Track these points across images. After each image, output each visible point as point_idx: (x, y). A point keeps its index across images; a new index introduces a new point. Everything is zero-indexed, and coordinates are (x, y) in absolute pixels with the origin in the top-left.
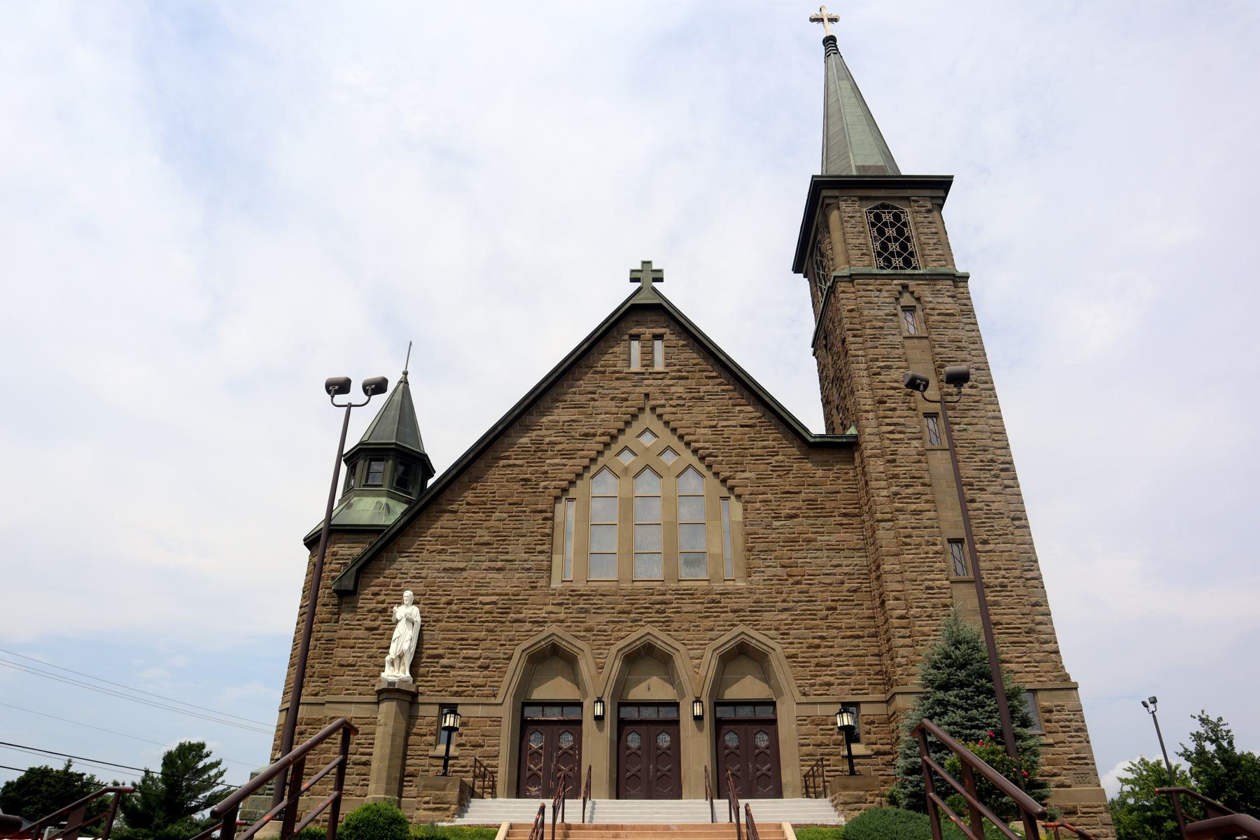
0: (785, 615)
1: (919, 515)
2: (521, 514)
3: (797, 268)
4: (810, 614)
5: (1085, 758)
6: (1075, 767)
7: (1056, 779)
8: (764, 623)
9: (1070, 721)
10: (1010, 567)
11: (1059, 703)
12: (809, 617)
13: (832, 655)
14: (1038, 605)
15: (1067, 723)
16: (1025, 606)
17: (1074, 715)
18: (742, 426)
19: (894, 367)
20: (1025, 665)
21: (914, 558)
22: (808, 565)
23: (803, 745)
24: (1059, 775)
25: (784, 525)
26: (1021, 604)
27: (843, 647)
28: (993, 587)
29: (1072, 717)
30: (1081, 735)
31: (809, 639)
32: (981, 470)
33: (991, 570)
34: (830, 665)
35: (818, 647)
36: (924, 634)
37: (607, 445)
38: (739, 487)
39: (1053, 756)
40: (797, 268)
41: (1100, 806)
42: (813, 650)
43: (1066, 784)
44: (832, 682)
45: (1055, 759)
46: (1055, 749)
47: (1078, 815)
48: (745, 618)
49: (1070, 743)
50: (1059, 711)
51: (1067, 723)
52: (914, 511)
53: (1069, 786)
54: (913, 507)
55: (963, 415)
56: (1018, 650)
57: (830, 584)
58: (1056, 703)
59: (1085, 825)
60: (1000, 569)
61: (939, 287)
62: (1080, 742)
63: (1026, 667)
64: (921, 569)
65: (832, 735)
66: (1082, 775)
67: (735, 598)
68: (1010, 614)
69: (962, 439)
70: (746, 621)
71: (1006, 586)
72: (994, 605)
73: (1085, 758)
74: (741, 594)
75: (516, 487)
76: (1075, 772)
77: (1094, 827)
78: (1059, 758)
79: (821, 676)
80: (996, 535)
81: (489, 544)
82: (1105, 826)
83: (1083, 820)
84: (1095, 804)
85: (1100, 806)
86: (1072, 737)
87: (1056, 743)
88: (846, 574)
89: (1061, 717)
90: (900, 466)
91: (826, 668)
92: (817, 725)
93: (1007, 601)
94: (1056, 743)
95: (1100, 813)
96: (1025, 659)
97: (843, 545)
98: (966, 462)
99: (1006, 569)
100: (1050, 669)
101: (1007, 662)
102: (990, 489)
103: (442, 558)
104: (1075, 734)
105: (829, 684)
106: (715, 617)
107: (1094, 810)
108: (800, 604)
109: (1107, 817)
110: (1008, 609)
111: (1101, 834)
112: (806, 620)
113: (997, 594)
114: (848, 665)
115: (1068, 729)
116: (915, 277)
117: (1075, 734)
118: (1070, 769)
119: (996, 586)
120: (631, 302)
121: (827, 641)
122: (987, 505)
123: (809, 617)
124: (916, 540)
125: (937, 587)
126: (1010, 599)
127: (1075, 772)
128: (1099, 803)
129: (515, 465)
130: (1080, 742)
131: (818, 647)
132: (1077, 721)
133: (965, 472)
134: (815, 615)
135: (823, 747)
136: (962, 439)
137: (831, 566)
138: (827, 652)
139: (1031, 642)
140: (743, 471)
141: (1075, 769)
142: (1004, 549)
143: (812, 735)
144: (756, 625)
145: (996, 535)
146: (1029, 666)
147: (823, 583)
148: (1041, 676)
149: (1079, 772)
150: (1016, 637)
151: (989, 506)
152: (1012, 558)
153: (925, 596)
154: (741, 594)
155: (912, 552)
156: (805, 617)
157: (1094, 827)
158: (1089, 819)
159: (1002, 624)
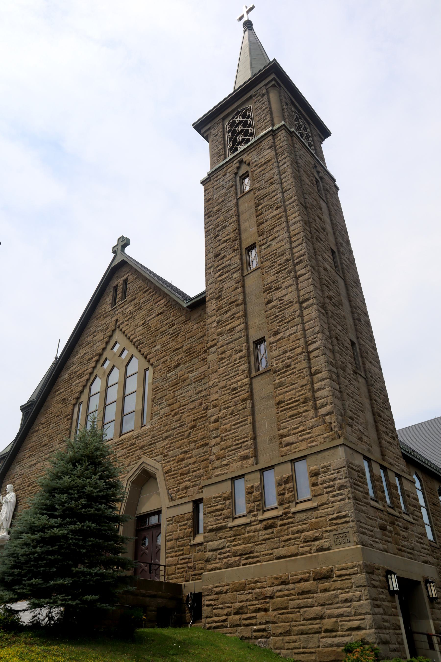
0: (166, 442)
1: (232, 331)
2: (175, 386)
3: (203, 183)
4: (180, 436)
5: (344, 517)
6: (335, 527)
7: (317, 543)
8: (155, 451)
9: (334, 479)
10: (294, 347)
11: (325, 464)
12: (180, 438)
13: (190, 464)
14: (318, 373)
15: (331, 483)
16: (304, 378)
17: (338, 472)
18: (158, 315)
19: (228, 225)
20: (300, 434)
21: (225, 368)
22: (183, 398)
23: (168, 541)
24: (321, 539)
25: (173, 374)
26: (301, 377)
27: (197, 455)
28: (279, 370)
29: (336, 475)
30: (344, 493)
31: (178, 455)
32: (278, 273)
33: (280, 356)
34: (188, 473)
35: (183, 460)
36: (226, 431)
37: (97, 361)
38: (152, 358)
39: (317, 520)
40: (203, 183)
41: (355, 566)
42: (180, 463)
43: (324, 547)
44: (188, 485)
45: (318, 522)
46: (319, 512)
47: (333, 579)
48: (146, 451)
49: (333, 502)
50: (325, 472)
51: (331, 483)
52: (229, 329)
53: (329, 549)
54: (228, 327)
55: (270, 234)
56: (295, 422)
57: (194, 408)
58: (322, 465)
59: (339, 589)
60: (286, 352)
61: (261, 147)
62: (341, 500)
63: (300, 436)
64: (231, 375)
65: (186, 529)
66: (341, 535)
67: (143, 438)
68: (291, 390)
69: (267, 254)
70: (146, 453)
71: (290, 366)
72: (279, 387)
73: (344, 517)
74: (146, 434)
75: (60, 405)
76: (335, 533)
77: (347, 590)
78: (322, 521)
79: (183, 483)
80: (285, 323)
81: (46, 444)
82: (360, 588)
83: (338, 584)
84: (350, 564)
85: (355, 566)
86: (334, 496)
87: (320, 506)
88: (203, 396)
89: (325, 478)
90: (225, 298)
91: (186, 476)
92: (178, 522)
93: (290, 379)
94: (320, 506)
95: (354, 574)
96: (301, 428)
97: (204, 375)
98: (268, 271)
99: (291, 350)
100: (320, 432)
101: (286, 436)
102: (284, 286)
103: (30, 460)
104: (338, 492)
105: (186, 488)
106: (132, 455)
107: (348, 572)
108: (175, 430)
109: (361, 578)
110: (290, 386)
111: (354, 597)
112: (178, 441)
113: (282, 375)
114: (199, 469)
115: (331, 489)
116: (246, 151)
117: (338, 492)
118: (330, 531)
119: (283, 369)
120: (111, 267)
121: (189, 454)
122: (280, 300)
123: (180, 438)
124: (229, 353)
125: (239, 386)
126: (292, 376)
127: (335, 533)
128: (354, 564)
129: (61, 392)
130: (341, 500)
131: (183, 460)
132: (340, 479)
133: (266, 280)
134: (183, 435)
135: (180, 540)
136: (267, 254)
137: (195, 394)
138: (187, 463)
139: (306, 411)
140: (155, 346)
141: (335, 530)
142: (291, 333)
143: (174, 531)
144: (151, 455)
145: (285, 323)
146: (303, 435)
147: (190, 409)
148: (312, 441)
149: (339, 532)
150: (295, 410)
151: (282, 300)
152: (297, 338)
153: (230, 398)
154: (146, 434)
155: (226, 363)
156: (177, 439)
157: (347, 590)
158: (344, 581)
159: (284, 402)
